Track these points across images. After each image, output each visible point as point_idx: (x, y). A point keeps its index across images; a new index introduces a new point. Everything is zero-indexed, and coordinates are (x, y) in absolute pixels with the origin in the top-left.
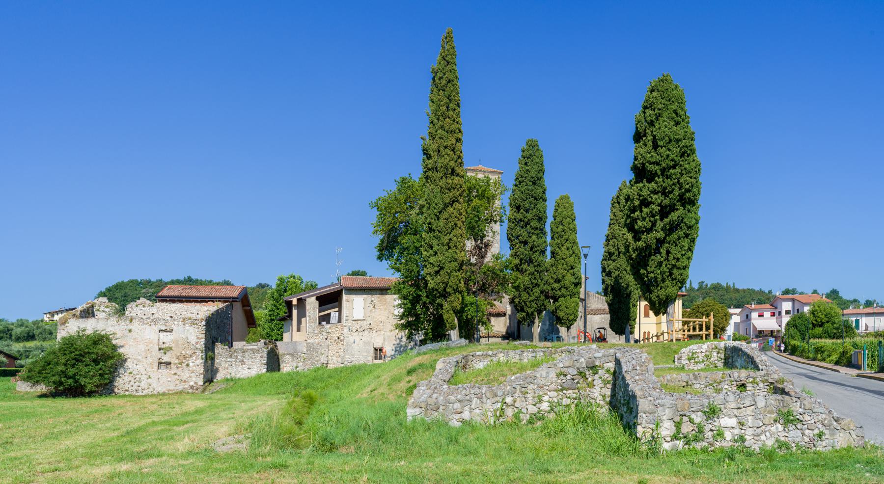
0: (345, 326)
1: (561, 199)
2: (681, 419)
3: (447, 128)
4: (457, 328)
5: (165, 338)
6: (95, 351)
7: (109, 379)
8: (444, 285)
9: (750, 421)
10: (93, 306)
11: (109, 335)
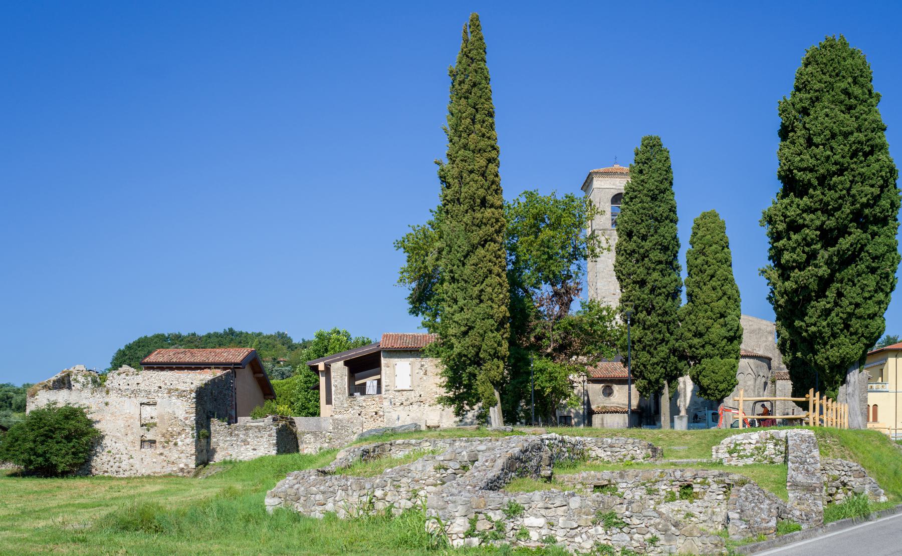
0: (385, 398)
1: (704, 216)
2: (477, 517)
3: (472, 147)
4: (499, 404)
5: (148, 411)
6: (66, 426)
7: (84, 458)
8: (475, 349)
9: (560, 521)
10: (69, 375)
11: (82, 409)
